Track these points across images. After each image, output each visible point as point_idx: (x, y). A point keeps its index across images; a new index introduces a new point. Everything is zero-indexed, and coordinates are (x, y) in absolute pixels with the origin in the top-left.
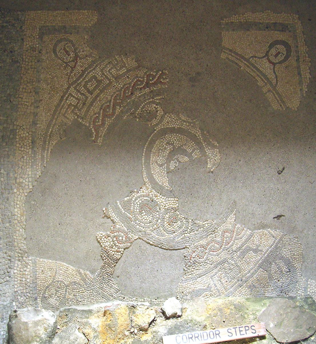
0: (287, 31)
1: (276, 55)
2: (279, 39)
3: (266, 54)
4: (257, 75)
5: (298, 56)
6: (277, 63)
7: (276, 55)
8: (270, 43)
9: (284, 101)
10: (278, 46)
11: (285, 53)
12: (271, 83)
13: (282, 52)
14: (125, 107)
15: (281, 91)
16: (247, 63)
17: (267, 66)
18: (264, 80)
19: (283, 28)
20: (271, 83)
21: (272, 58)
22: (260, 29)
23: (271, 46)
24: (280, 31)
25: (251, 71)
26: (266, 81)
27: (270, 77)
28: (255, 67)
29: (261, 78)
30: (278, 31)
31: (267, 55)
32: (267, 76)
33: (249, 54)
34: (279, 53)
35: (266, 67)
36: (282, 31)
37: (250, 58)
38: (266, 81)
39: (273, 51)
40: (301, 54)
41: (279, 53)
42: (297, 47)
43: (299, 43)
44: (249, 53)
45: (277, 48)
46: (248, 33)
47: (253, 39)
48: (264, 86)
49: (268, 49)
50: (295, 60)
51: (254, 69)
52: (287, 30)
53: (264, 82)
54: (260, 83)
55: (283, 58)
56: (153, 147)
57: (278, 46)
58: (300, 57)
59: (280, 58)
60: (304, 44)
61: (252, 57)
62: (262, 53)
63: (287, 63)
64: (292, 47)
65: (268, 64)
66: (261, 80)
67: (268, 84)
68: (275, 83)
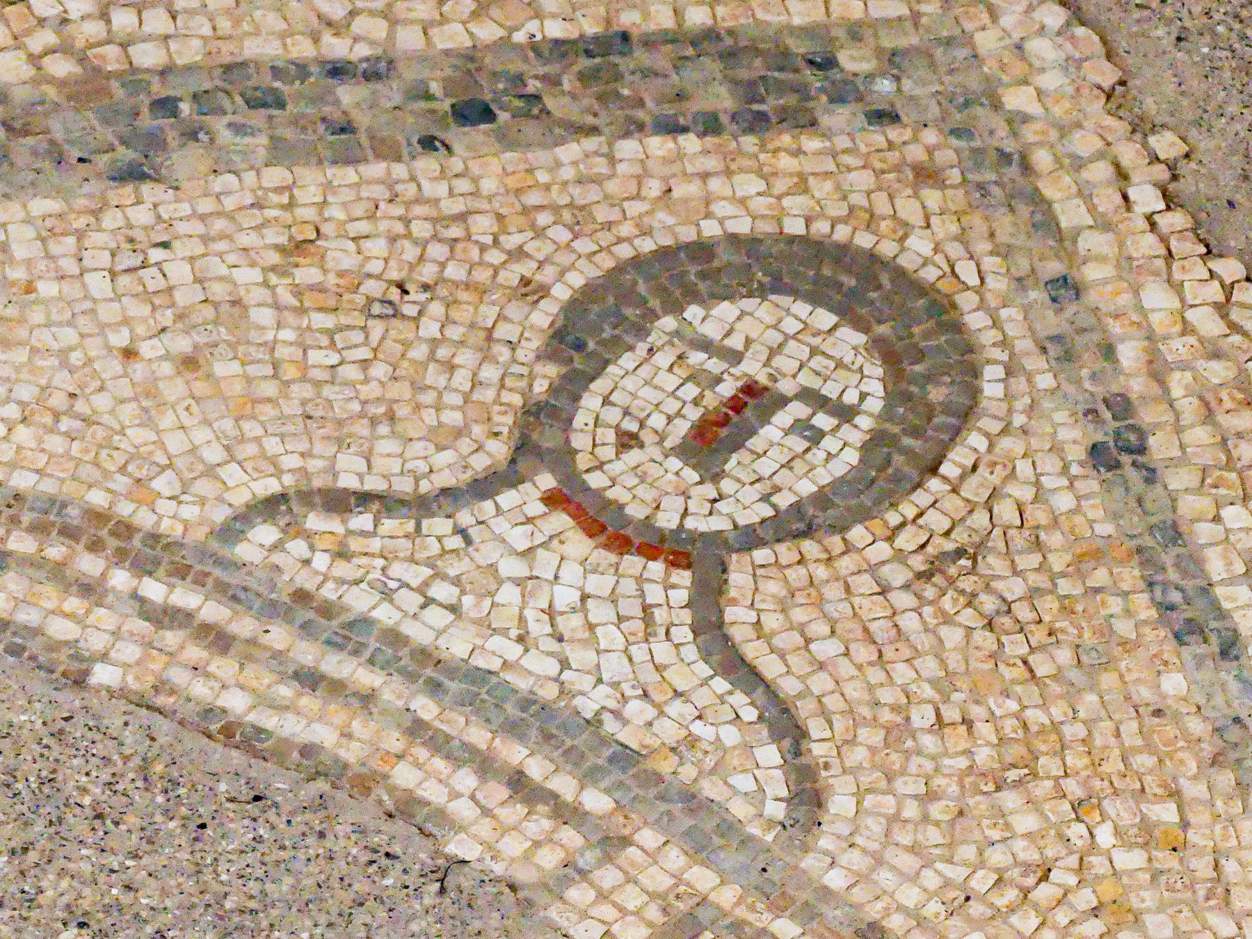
0: (839, 118)
1: (715, 439)
2: (711, 229)
3: (523, 447)
4: (416, 728)
5: (1121, 406)
6: (750, 538)
7: (715, 439)
8: (561, 293)
9: (755, 443)
10: (726, 310)
11: (869, 388)
12: (703, 826)
13: (806, 379)
14: (1024, 289)
15: (910, 896)
16: (186, 597)
17: (565, 596)
18: (564, 786)
19: (750, 91)
20: (703, 826)
21: (654, 487)
22: (343, 140)
23: (586, 338)
24: (710, 125)
25: (285, 691)
26: (596, 801)
27: (668, 731)
28: (350, 634)
29: (484, 764)
30: (673, 128)
31: (538, 436)
32: (594, 723)
33: (210, 472)
34: (754, 400)
35: (540, 602)
36: (758, 123)
37: (231, 531)
38: (596, 801)
39: (650, 385)
40: (1157, 370)
41: (754, 400)
42: (1066, 288)
43: (1094, 242)
44: (213, 454)
45: (705, 345)
46: (140, 208)
47: (248, 275)
48: (572, 871)
49: (552, 370)
50: (1077, 453)
51: (336, 665)
52: (838, 98)
53: (566, 813)
54: (492, 836)
55: (852, 457)
56: (598, 493)
57: (715, 319)
58: (1148, 416)
59: (781, 464)
60: (1187, 247)
61: (271, 506)
62: (443, 438)
63: (933, 508)
64: (967, 301)
65: (589, 568)
66: (497, 792)
67: (649, 838)
68: (776, 810)
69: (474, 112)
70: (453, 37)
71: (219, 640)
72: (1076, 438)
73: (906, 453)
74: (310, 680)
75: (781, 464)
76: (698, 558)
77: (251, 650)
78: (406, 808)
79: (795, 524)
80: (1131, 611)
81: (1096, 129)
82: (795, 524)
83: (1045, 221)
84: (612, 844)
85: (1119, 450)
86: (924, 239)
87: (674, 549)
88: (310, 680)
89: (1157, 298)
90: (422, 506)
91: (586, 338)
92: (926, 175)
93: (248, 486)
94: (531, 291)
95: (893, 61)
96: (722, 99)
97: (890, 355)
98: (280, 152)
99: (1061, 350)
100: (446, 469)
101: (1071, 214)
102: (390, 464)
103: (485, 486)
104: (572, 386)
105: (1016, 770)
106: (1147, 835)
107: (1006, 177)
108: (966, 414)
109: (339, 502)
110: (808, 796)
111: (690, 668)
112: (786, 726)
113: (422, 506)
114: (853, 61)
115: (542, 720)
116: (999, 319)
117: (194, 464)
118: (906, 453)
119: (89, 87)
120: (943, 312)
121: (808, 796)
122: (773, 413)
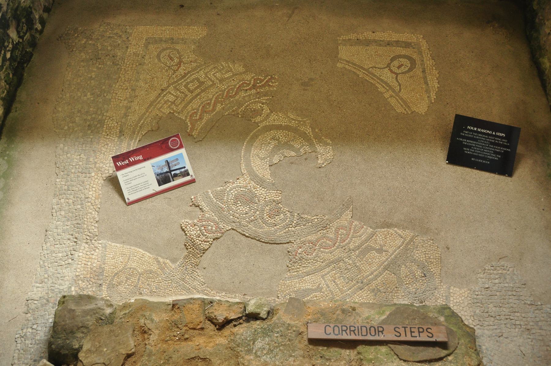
1: (399, 67)
5: (424, 68)
6: (400, 73)
7: (399, 67)
12: (394, 91)
18: (395, 254)
20: (394, 91)
22: (380, 45)
23: (392, 60)
24: (403, 47)
29: (382, 85)
31: (388, 66)
35: (387, 75)
36: (406, 48)
39: (396, 63)
40: (427, 66)
42: (423, 61)
53: (386, 89)
54: (381, 89)
57: (400, 60)
59: (403, 69)
61: (371, 67)
69: (388, 44)
70: (388, 39)
71: (367, 75)
72: (421, 70)
73: (410, 70)
74: (372, 78)
75: (403, 69)
76: (397, 74)
77: (369, 76)
78: (376, 87)
79: (403, 73)
80: (422, 81)
81: (427, 51)
82: (403, 73)
83: (422, 57)
84: (388, 91)
85: (424, 71)
86: (415, 56)
87: (396, 73)
88: (372, 78)
89: (428, 62)
90: (381, 69)
91: (392, 60)
92: (415, 52)
93: (370, 66)
94: (390, 56)
95: (415, 45)
96: (404, 46)
97: (411, 63)
98: (376, 45)
99: (422, 65)
100: (383, 66)
101: (424, 56)
102: (380, 66)
103: (385, 68)
104: (391, 62)
105: (413, 90)
106: (420, 95)
107: (420, 53)
108: (415, 68)
109: (376, 68)
110: (400, 90)
111: (395, 81)
112: (400, 85)
113: (381, 69)
114: (413, 44)
115: (386, 83)
116: (418, 62)
117: (368, 64)
118: (410, 70)
119: (366, 40)
120: (415, 61)
121: (400, 90)
122: (358, 346)
